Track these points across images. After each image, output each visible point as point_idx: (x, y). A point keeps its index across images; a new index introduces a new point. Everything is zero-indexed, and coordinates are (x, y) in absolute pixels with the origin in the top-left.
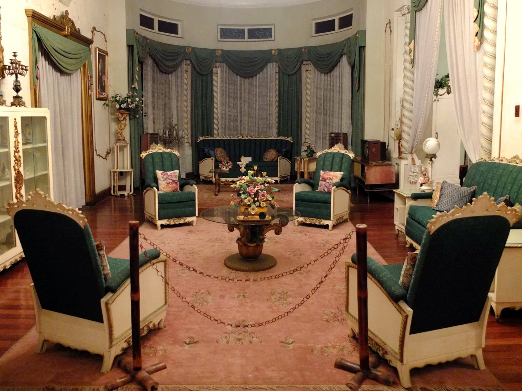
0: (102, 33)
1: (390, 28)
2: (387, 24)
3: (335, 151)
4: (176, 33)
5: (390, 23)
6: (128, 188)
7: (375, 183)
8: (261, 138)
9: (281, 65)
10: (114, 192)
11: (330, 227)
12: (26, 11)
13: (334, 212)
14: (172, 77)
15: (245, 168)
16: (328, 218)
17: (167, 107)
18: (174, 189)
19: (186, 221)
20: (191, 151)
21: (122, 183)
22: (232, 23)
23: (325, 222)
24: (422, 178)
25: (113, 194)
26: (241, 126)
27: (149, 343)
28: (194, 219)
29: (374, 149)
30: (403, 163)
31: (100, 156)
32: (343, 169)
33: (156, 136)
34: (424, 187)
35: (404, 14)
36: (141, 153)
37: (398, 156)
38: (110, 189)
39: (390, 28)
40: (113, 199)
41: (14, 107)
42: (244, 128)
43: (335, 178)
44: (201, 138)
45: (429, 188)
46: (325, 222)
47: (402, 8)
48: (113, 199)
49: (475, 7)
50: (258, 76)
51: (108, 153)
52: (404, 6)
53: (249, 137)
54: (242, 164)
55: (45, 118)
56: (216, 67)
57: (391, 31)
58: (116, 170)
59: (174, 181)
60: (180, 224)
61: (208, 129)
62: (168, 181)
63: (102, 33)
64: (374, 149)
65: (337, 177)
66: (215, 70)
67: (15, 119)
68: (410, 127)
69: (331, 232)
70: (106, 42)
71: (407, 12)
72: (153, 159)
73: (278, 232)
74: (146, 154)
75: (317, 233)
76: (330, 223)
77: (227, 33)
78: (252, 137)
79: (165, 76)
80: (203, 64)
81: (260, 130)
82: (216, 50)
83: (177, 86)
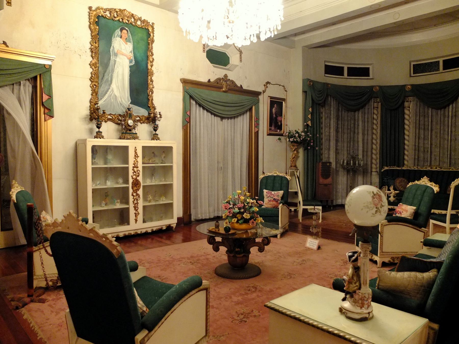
4: (368, 75)
8: (451, 170)
12: (181, 80)
14: (359, 115)
15: (394, 197)
17: (352, 140)
18: (274, 206)
20: (378, 179)
22: (425, 57)
26: (431, 158)
41: (96, 139)
42: (435, 159)
43: (404, 212)
44: (386, 168)
50: (451, 106)
53: (438, 168)
54: (391, 193)
55: (171, 148)
56: (408, 101)
59: (274, 199)
61: (399, 160)
62: (270, 199)
65: (407, 211)
66: (406, 104)
67: (135, 147)
70: (286, 91)
72: (267, 181)
73: (261, 250)
77: (419, 68)
78: (441, 168)
79: (351, 114)
80: (392, 100)
81: (453, 162)
82: (405, 85)
83: (364, 122)
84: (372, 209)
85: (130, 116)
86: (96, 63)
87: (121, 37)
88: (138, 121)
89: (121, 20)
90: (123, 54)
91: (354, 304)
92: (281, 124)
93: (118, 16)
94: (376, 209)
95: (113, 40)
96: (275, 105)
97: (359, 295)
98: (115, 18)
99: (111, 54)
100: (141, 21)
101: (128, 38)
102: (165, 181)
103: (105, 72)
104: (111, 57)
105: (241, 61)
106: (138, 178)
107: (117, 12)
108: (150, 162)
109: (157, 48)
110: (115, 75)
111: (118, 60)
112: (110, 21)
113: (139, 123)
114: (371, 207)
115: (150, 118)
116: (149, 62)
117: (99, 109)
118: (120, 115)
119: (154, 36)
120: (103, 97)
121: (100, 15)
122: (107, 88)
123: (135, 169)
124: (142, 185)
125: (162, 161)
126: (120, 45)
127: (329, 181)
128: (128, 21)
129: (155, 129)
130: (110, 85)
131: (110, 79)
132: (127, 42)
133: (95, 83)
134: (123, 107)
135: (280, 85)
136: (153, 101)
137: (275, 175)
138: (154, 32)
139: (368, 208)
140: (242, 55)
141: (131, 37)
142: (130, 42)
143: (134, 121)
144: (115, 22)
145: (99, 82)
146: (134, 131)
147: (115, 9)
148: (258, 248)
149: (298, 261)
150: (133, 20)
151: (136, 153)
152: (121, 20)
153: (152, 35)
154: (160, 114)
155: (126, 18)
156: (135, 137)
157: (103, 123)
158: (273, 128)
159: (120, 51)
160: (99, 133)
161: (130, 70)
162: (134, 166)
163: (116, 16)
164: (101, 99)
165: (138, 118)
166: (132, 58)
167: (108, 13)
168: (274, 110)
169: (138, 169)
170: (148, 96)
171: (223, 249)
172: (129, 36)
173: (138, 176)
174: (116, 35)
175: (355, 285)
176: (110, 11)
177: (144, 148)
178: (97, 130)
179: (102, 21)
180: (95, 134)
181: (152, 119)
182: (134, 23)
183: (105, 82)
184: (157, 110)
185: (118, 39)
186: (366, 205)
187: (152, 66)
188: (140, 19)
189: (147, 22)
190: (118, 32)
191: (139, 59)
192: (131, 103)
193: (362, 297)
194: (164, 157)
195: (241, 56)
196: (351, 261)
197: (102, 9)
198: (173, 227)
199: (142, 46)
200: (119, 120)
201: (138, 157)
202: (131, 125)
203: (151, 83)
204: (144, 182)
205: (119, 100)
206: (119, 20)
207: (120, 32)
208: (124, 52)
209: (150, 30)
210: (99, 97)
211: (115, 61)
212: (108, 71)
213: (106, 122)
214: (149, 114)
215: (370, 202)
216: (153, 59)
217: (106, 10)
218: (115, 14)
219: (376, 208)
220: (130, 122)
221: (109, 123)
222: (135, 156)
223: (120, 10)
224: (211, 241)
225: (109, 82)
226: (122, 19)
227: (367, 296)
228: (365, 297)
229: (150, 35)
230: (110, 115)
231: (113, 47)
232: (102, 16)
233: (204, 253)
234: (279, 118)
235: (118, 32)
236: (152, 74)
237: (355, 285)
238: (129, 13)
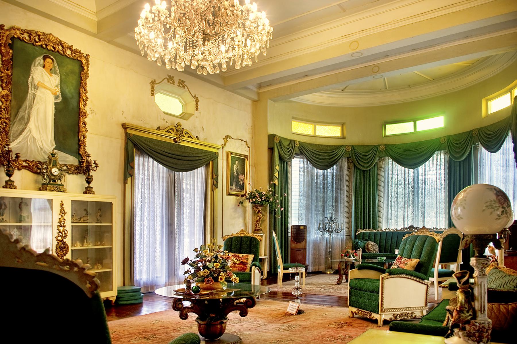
33: (302, 228)
44: (361, 231)
67: (62, 202)
73: (243, 314)
84: (497, 210)
85: (55, 164)
86: (7, 95)
87: (44, 67)
88: (65, 170)
89: (44, 46)
90: (46, 88)
91: (467, 338)
92: (243, 184)
93: (40, 40)
94: (503, 210)
95: (33, 69)
96: (237, 162)
97: (475, 325)
98: (37, 42)
99: (30, 86)
100: (72, 51)
101: (53, 69)
102: (101, 245)
103: (20, 107)
104: (30, 90)
105: (197, 109)
106: (65, 240)
107: (39, 36)
108: (82, 221)
109: (91, 84)
110: (34, 113)
111: (38, 93)
112: (28, 45)
113: (67, 174)
114: (496, 207)
115: (81, 167)
116: (82, 100)
117: (11, 151)
118: (40, 162)
119: (88, 70)
120: (16, 139)
121: (15, 36)
122: (21, 127)
123: (61, 229)
124: (70, 248)
125: (98, 220)
126: (42, 75)
127: (300, 246)
128: (54, 48)
129: (89, 180)
130: (26, 124)
131: (26, 116)
132: (52, 73)
133: (6, 121)
134: (45, 152)
135: (242, 140)
136: (86, 148)
137: (242, 235)
138: (89, 66)
139: (492, 208)
140: (199, 103)
141: (57, 68)
142: (55, 73)
143: (61, 170)
144: (37, 48)
145: (11, 119)
146: (59, 182)
147: (36, 32)
148: (239, 312)
149: (283, 327)
150: (60, 47)
151: (62, 208)
152: (44, 46)
153: (86, 68)
154: (95, 163)
155: (52, 45)
156: (61, 189)
157: (16, 172)
158: (234, 187)
159: (42, 83)
160: (9, 183)
161: (55, 109)
162: (59, 224)
163: (37, 40)
164: (13, 141)
165: (65, 168)
166: (59, 93)
167: (26, 35)
168: (235, 168)
169: (65, 228)
170: (79, 140)
171: (193, 316)
172: (55, 67)
173: (65, 237)
174: (37, 63)
175: (467, 314)
176: (29, 33)
177: (74, 202)
178: (7, 178)
179: (18, 44)
180: (4, 184)
181: (84, 168)
182: (62, 52)
183: (20, 120)
184: (92, 159)
185: (40, 68)
186: (488, 204)
187: (85, 105)
188: (70, 48)
189: (80, 53)
190: (40, 60)
191: (69, 95)
192: (55, 149)
193: (480, 328)
194: (100, 216)
195: (197, 104)
196: (462, 283)
197: (19, 29)
198: (112, 301)
199: (73, 80)
200: (38, 168)
201: (65, 213)
202: (55, 174)
203: (83, 125)
204: (73, 245)
205: (39, 143)
206: (42, 46)
207: (42, 61)
208: (47, 84)
209: (84, 63)
210: (11, 138)
211: (35, 96)
212: (24, 107)
213: (19, 169)
214: (81, 163)
215: (494, 201)
216: (87, 98)
217: (23, 32)
218: (37, 38)
219: (503, 208)
220: (55, 171)
221: (24, 172)
222: (61, 212)
223: (44, 34)
224: (176, 305)
225: (26, 121)
226: (46, 45)
227: (486, 326)
228: (483, 327)
229: (83, 68)
230: (25, 161)
231: (33, 77)
232: (19, 38)
233: (161, 327)
234: (241, 177)
235: (40, 60)
236: (85, 115)
237: (467, 314)
238: (57, 39)
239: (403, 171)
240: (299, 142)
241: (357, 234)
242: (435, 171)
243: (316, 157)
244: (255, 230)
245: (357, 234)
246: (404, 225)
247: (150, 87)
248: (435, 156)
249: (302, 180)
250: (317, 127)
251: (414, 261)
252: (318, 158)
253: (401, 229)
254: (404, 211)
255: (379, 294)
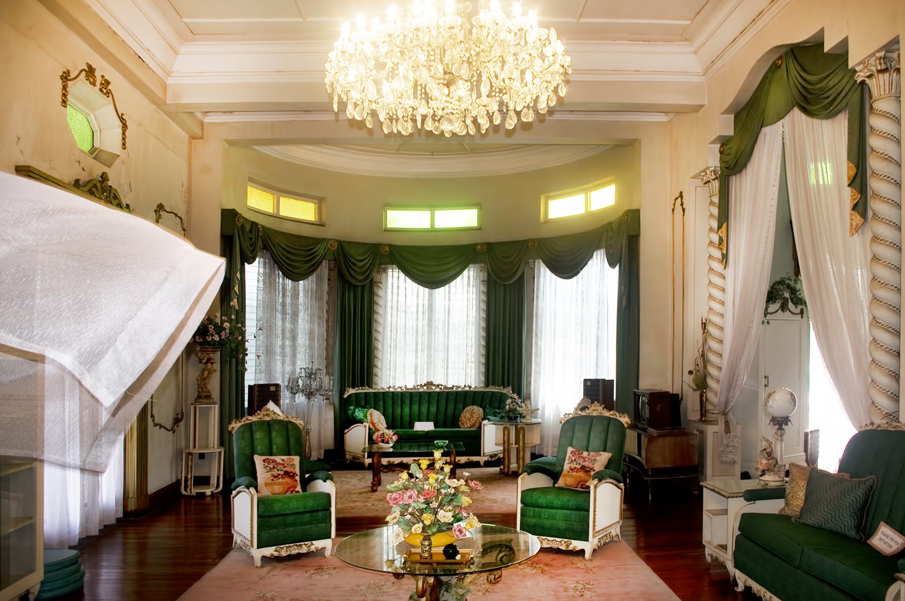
0: (176, 215)
1: (682, 204)
2: (676, 199)
3: (595, 414)
5: (681, 196)
6: (214, 481)
7: (662, 466)
9: (493, 271)
10: (186, 490)
11: (588, 555)
13: (594, 526)
16: (583, 535)
19: (313, 548)
21: (202, 473)
23: (577, 545)
24: (764, 461)
25: (184, 492)
27: (459, 109)
28: (326, 544)
29: (660, 406)
30: (710, 430)
31: (161, 426)
32: (609, 445)
33: (272, 389)
34: (766, 478)
35: (709, 182)
36: (230, 423)
37: (699, 417)
38: (178, 482)
39: (682, 204)
40: (183, 501)
44: (351, 391)
45: (777, 478)
46: (577, 545)
47: (704, 171)
48: (183, 501)
49: (849, 159)
51: (177, 421)
52: (708, 168)
57: (684, 210)
58: (191, 449)
60: (299, 553)
63: (176, 215)
64: (660, 406)
68: (720, 368)
69: (589, 565)
71: (714, 177)
74: (239, 424)
75: (564, 565)
76: (587, 546)
239: (415, 291)
240: (263, 227)
241: (345, 396)
242: (465, 296)
243: (287, 258)
244: (199, 397)
245: (345, 396)
246: (416, 381)
247: (59, 84)
248: (465, 272)
249: (260, 297)
250: (282, 200)
251: (605, 457)
252: (287, 258)
253: (414, 388)
254: (416, 357)
255: (588, 511)
